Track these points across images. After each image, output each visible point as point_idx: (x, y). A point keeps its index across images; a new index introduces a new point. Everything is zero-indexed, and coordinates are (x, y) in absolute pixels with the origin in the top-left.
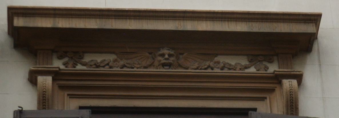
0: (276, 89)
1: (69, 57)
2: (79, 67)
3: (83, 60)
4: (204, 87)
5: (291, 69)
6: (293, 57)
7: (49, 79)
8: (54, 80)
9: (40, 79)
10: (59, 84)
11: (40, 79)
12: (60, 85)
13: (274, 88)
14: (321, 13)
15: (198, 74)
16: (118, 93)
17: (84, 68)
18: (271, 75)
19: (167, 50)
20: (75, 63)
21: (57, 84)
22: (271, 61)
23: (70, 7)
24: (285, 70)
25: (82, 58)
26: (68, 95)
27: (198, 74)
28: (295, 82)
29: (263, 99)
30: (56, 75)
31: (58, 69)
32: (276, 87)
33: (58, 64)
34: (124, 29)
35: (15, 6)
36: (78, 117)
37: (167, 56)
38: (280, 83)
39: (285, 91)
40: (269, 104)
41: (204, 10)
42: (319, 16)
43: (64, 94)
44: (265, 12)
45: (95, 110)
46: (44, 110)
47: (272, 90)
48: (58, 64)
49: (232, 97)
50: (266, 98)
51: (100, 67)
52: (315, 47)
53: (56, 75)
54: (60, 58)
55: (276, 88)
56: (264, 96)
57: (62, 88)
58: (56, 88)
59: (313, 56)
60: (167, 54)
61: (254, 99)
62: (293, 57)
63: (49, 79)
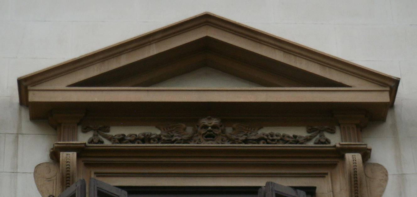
1: (94, 130)
2: (107, 143)
4: (292, 163)
5: (359, 141)
6: (361, 131)
7: (73, 155)
8: (78, 156)
9: (63, 155)
10: (85, 161)
11: (63, 155)
15: (225, 148)
16: (283, 171)
17: (107, 143)
18: (332, 148)
20: (212, 133)
21: (83, 161)
22: (332, 132)
24: (352, 143)
25: (108, 131)
26: (95, 173)
27: (225, 148)
28: (358, 156)
29: (323, 176)
30: (81, 151)
31: (83, 145)
32: (338, 162)
33: (83, 138)
34: (326, 77)
35: (52, 66)
36: (119, 196)
37: (210, 128)
38: (343, 158)
39: (347, 167)
40: (330, 184)
42: (397, 82)
43: (91, 172)
45: (130, 190)
46: (68, 188)
47: (334, 165)
48: (83, 138)
49: (264, 174)
50: (327, 174)
52: (389, 120)
53: (81, 151)
54: (85, 131)
56: (325, 171)
57: (88, 165)
58: (82, 164)
60: (210, 126)
62: (361, 131)
63: (73, 155)
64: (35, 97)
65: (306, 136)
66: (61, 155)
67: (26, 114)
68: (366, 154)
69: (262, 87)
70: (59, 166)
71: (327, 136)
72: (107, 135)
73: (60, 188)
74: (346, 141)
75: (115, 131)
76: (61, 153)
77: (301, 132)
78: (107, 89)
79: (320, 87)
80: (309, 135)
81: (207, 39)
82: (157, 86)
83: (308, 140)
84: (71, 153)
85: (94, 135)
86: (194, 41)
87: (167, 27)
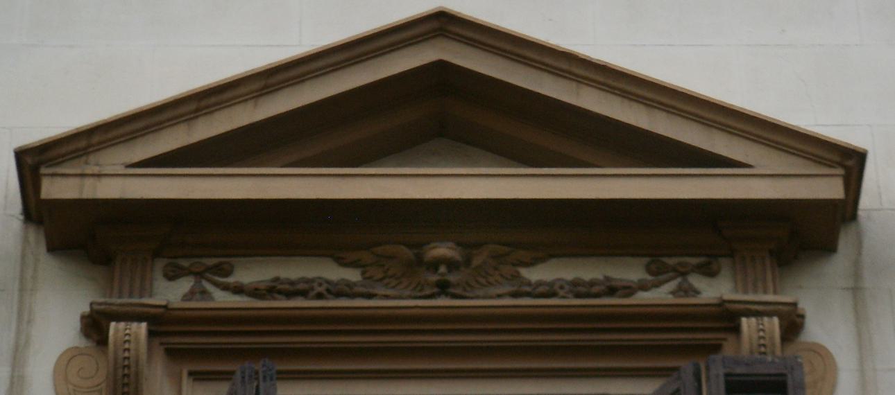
0: (725, 343)
2: (222, 299)
3: (231, 280)
8: (151, 334)
12: (169, 346)
13: (719, 342)
14: (864, 150)
18: (713, 309)
19: (448, 248)
21: (162, 344)
22: (709, 272)
23: (49, 138)
26: (191, 374)
32: (725, 339)
38: (737, 330)
41: (346, 39)
43: (181, 373)
44: (101, 123)
51: (277, 296)
52: (845, 242)
54: (173, 275)
55: (724, 343)
57: (174, 354)
59: (838, 265)
61: (492, 50)
64: (56, 188)
65: (639, 281)
66: (111, 332)
67: (37, 240)
68: (793, 325)
69: (520, 167)
70: (105, 353)
71: (696, 281)
72: (229, 284)
73: (22, 214)
74: (746, 292)
75: (252, 273)
76: (113, 324)
77: (630, 271)
78: (373, 173)
79: (650, 167)
80: (649, 278)
81: (441, 67)
82: (380, 166)
83: (644, 287)
84: (134, 325)
85: (196, 282)
86: (394, 76)
87: (361, 36)
